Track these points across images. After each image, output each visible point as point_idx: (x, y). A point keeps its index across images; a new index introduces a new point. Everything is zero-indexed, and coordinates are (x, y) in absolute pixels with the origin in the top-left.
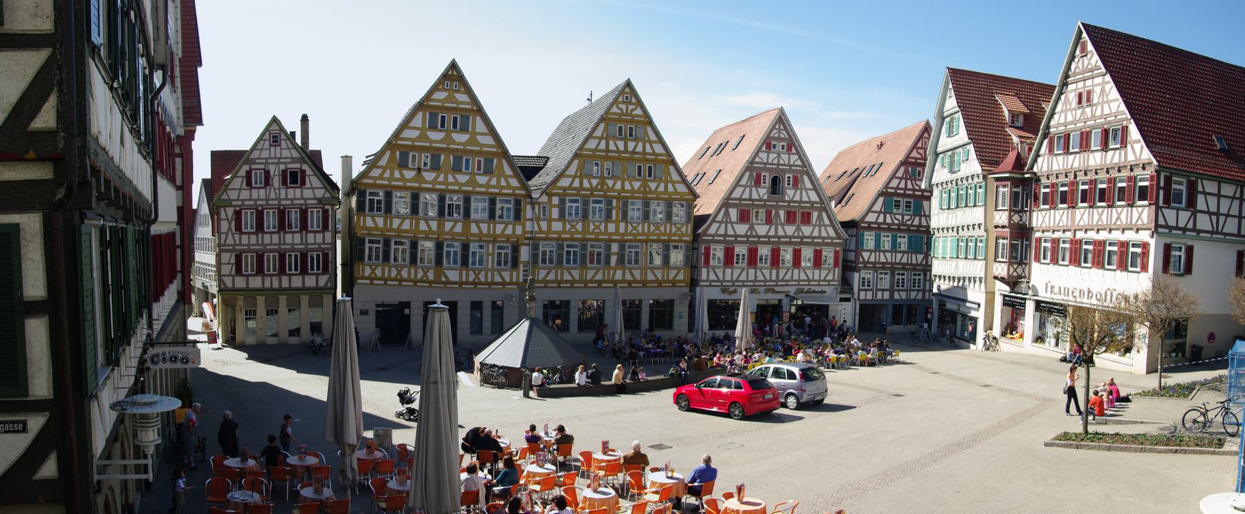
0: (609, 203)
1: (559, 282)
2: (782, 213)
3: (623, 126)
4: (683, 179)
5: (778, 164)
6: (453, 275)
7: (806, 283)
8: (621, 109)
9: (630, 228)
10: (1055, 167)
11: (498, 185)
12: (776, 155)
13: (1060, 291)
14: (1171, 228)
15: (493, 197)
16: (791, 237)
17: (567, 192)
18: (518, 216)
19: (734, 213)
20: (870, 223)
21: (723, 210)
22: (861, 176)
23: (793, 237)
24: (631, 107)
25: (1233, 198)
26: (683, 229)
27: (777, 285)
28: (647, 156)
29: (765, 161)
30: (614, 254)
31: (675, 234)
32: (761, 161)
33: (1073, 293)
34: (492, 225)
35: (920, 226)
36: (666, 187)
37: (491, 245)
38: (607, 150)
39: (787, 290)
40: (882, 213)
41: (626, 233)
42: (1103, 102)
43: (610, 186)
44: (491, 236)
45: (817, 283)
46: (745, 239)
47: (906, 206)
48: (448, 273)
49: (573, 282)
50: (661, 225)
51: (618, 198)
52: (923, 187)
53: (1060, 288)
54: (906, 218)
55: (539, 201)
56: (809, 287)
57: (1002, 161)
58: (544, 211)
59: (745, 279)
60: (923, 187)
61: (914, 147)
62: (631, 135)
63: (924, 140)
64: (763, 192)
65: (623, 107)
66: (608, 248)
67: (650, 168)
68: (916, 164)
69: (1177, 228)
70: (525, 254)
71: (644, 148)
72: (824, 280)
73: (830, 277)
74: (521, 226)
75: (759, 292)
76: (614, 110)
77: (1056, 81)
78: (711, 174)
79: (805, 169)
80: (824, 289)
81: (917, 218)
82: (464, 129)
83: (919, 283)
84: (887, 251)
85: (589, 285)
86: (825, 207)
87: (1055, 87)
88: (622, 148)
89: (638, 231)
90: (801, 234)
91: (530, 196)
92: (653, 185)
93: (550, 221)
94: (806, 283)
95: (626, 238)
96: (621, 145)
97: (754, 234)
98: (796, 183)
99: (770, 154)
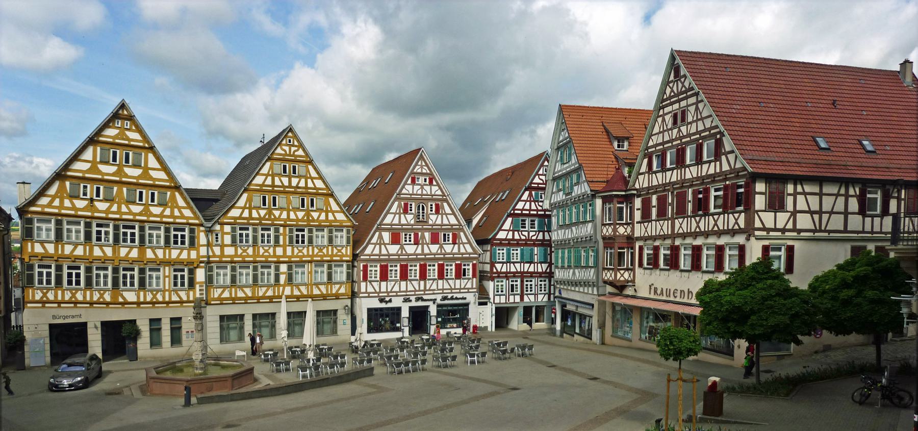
6: (131, 296)
7: (450, 291)
8: (285, 151)
10: (655, 183)
11: (172, 216)
14: (769, 230)
24: (293, 149)
26: (344, 251)
27: (425, 294)
30: (283, 273)
32: (407, 192)
35: (544, 239)
36: (327, 216)
38: (273, 185)
40: (511, 231)
41: (293, 256)
45: (458, 291)
48: (125, 294)
54: (531, 234)
56: (452, 295)
65: (287, 148)
66: (277, 269)
69: (776, 230)
70: (200, 275)
71: (306, 183)
72: (464, 288)
73: (469, 286)
74: (196, 252)
75: (411, 301)
82: (136, 165)
86: (462, 228)
89: (303, 253)
90: (443, 251)
93: (222, 246)
94: (450, 291)
95: (292, 259)
96: (285, 181)
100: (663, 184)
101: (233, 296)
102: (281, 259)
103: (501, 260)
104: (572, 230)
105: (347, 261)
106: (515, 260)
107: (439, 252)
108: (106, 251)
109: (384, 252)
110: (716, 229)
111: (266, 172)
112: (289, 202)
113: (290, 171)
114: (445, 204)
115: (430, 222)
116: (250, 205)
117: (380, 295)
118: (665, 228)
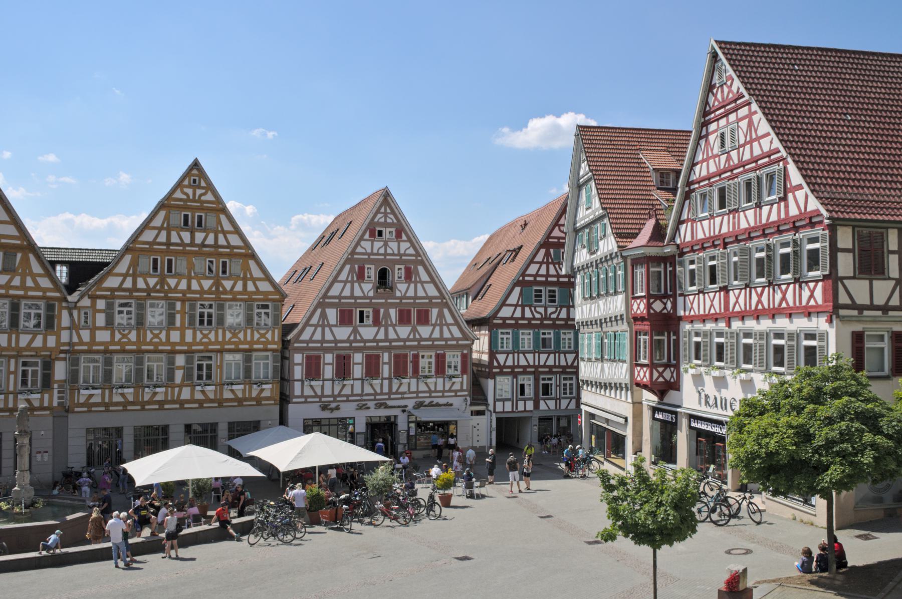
0: (172, 306)
1: (107, 405)
2: (393, 312)
3: (203, 215)
5: (386, 254)
7: (428, 395)
9: (199, 336)
10: (700, 236)
12: (382, 243)
13: (716, 403)
14: (861, 308)
15: (16, 301)
16: (404, 340)
17: (116, 293)
18: (50, 324)
19: (332, 315)
20: (504, 319)
21: (319, 311)
22: (501, 263)
23: (408, 340)
24: (199, 192)
27: (390, 399)
29: (369, 251)
31: (258, 342)
32: (364, 251)
33: (731, 406)
34: (14, 336)
36: (245, 286)
37: (13, 361)
38: (168, 243)
39: (403, 405)
41: (194, 343)
42: (751, 142)
43: (173, 286)
44: (13, 349)
45: (441, 394)
46: (348, 345)
47: (550, 296)
49: (126, 404)
51: (183, 301)
53: (716, 398)
54: (550, 310)
58: (86, 318)
59: (350, 393)
65: (190, 191)
66: (171, 361)
69: (872, 307)
70: (60, 371)
71: (216, 239)
72: (450, 391)
73: (457, 387)
75: (368, 408)
77: (688, 122)
79: (419, 258)
80: (450, 400)
83: (571, 389)
85: (147, 407)
86: (447, 302)
87: (691, 132)
89: (209, 339)
92: (228, 284)
93: (94, 329)
94: (428, 395)
95: (194, 348)
96: (186, 236)
97: (358, 338)
99: (375, 243)
100: (711, 237)
101: (107, 400)
102: (177, 348)
103: (505, 349)
104: (598, 306)
105: (273, 350)
106: (567, 349)
110: (784, 305)
112: (191, 266)
113: (193, 222)
114: (421, 269)
115: (398, 294)
117: (323, 399)
118: (716, 302)
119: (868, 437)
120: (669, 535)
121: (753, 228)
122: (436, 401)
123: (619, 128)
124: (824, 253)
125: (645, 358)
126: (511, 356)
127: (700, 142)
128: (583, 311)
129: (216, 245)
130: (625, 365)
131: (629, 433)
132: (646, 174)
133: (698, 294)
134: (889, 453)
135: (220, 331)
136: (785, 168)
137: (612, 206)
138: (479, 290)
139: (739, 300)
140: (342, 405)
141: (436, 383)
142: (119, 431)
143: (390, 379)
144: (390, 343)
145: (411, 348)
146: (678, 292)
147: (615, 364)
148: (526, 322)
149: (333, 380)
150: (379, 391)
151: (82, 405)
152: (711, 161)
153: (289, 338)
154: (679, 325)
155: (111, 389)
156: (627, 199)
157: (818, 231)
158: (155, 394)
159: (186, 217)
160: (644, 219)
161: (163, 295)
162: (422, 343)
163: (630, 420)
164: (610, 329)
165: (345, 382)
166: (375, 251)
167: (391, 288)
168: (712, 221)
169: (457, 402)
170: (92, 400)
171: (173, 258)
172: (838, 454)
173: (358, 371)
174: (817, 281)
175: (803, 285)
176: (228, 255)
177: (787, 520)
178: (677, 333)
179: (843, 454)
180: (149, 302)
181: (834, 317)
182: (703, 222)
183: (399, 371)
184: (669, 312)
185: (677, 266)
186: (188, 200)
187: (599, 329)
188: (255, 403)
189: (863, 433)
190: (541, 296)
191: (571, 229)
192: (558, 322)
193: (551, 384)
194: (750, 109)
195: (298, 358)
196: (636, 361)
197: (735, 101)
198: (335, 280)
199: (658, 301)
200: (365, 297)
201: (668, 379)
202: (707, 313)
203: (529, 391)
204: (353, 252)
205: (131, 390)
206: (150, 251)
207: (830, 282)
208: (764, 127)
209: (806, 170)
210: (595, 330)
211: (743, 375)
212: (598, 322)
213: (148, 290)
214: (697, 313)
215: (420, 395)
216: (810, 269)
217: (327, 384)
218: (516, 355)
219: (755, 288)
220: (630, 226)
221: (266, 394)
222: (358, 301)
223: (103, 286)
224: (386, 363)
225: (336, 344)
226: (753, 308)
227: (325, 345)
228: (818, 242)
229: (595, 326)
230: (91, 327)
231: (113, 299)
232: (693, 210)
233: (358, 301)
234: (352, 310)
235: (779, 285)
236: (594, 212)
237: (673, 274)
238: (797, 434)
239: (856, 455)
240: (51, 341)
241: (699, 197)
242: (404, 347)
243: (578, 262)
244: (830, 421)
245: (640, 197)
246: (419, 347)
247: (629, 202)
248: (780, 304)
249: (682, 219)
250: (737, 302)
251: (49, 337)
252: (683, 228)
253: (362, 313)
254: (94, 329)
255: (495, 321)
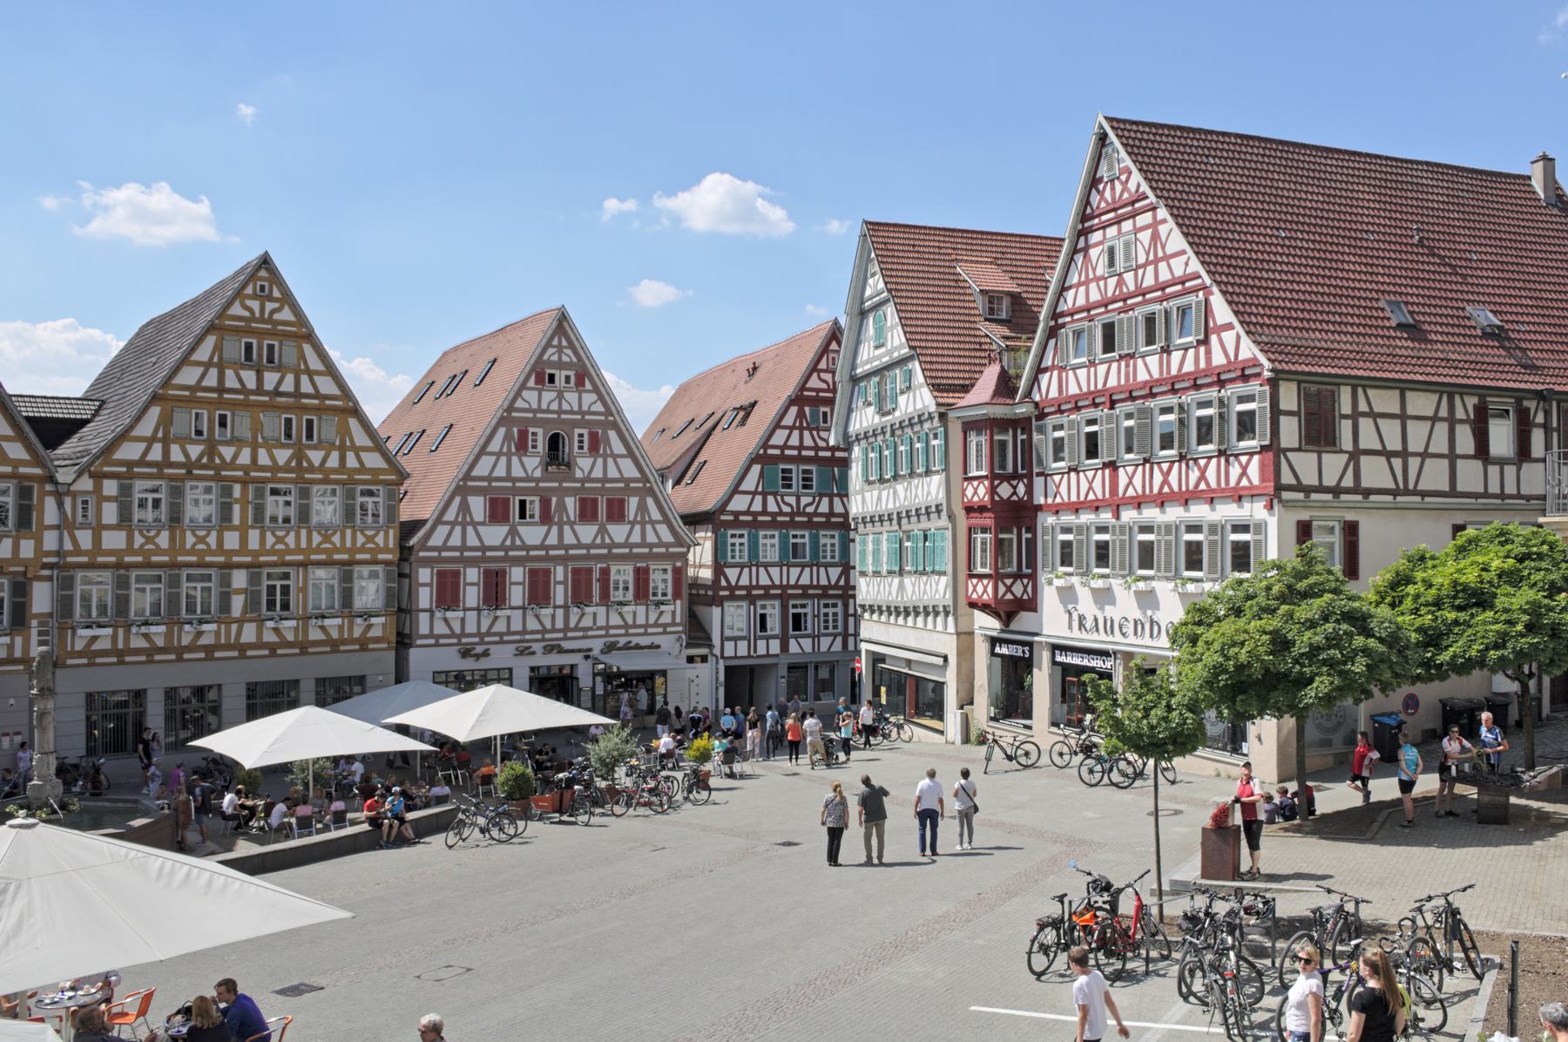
0: (227, 492)
1: (120, 654)
2: (570, 503)
4: (379, 445)
5: (560, 411)
7: (623, 631)
8: (250, 310)
10: (1073, 390)
12: (555, 394)
14: (1308, 490)
16: (588, 547)
18: (25, 519)
19: (478, 506)
20: (736, 514)
21: (457, 500)
22: (719, 428)
23: (593, 545)
24: (269, 306)
25: (1434, 419)
27: (566, 638)
28: (304, 401)
29: (535, 406)
31: (362, 550)
35: (831, 513)
36: (343, 459)
38: (221, 389)
39: (585, 647)
40: (760, 493)
41: (263, 550)
42: (1156, 261)
43: (228, 459)
45: (642, 631)
50: (335, 533)
51: (244, 482)
52: (832, 443)
53: (1096, 620)
55: (72, 488)
57: (973, 385)
59: (505, 630)
60: (832, 443)
61: (814, 369)
62: (271, 360)
63: (831, 355)
64: (533, 463)
65: (255, 305)
66: (226, 581)
67: (310, 423)
68: (817, 402)
69: (1321, 489)
70: (41, 598)
71: (297, 383)
72: (656, 625)
73: (666, 619)
75: (533, 653)
76: (236, 310)
77: (1062, 226)
78: (434, 433)
79: (611, 418)
80: (657, 640)
81: (825, 500)
83: (835, 621)
84: (773, 565)
85: (186, 656)
86: (651, 488)
87: (1063, 240)
88: (251, 383)
89: (286, 544)
91: (51, 479)
92: (315, 457)
93: (98, 529)
94: (623, 631)
95: (262, 559)
96: (249, 378)
98: (595, 445)
100: (1090, 393)
101: (120, 645)
102: (235, 559)
103: (737, 560)
104: (895, 492)
105: (387, 563)
106: (829, 559)
107: (598, 541)
108: (482, 534)
109: (472, 541)
110: (1203, 486)
111: (205, 358)
112: (257, 428)
113: (260, 355)
114: (612, 434)
115: (579, 474)
116: (166, 435)
117: (464, 640)
118: (1097, 485)
119: (1359, 641)
120: (1184, 744)
121: (1157, 380)
122: (635, 640)
123: (925, 228)
124: (1263, 416)
125: (983, 565)
126: (746, 570)
127: (1076, 257)
128: (863, 501)
129: (298, 394)
130: (944, 579)
131: (951, 679)
132: (967, 298)
133: (1068, 473)
134: (1383, 659)
135: (304, 533)
136: (1207, 301)
137: (923, 344)
138: (686, 468)
139: (1132, 480)
140: (493, 648)
141: (635, 613)
142: (139, 695)
143: (566, 607)
144: (567, 551)
145: (599, 558)
146: (1036, 470)
147: (925, 578)
148: (769, 518)
149: (478, 610)
150: (549, 626)
151: (80, 654)
152: (1093, 286)
153: (411, 543)
154: (1036, 517)
155: (128, 627)
156: (944, 334)
157: (1254, 387)
158: (199, 634)
159: (249, 347)
160: (980, 364)
161: (212, 472)
162: (615, 551)
163: (953, 660)
164: (916, 527)
165: (499, 613)
166: (544, 406)
167: (568, 465)
168: (1092, 369)
169: (667, 642)
170: (96, 646)
171: (229, 414)
172: (1324, 662)
173: (517, 595)
174: (1251, 454)
175: (1232, 459)
176: (317, 410)
177: (1209, 777)
178: (1032, 529)
179: (1330, 663)
180: (189, 484)
181: (1275, 501)
182: (1078, 371)
183: (580, 596)
184: (1021, 500)
185: (1034, 434)
186: (253, 319)
187: (897, 528)
188: (357, 647)
189: (1352, 637)
190: (791, 479)
191: (846, 377)
192: (815, 519)
193: (805, 614)
194: (1155, 217)
195: (424, 575)
196: (970, 570)
197: (1133, 203)
198: (482, 451)
199: (1005, 484)
200: (528, 479)
201: (1019, 596)
202: (1082, 499)
203: (774, 625)
204: (511, 408)
205: (162, 629)
206: (192, 401)
207: (1270, 455)
208: (1176, 240)
209: (1237, 304)
210: (888, 528)
211: (1141, 585)
212: (895, 516)
213: (189, 466)
214: (1066, 500)
215: (612, 632)
216: (1240, 437)
217: (470, 618)
218: (754, 569)
219: (1159, 463)
220: (950, 375)
221: (376, 632)
222: (518, 484)
223: (114, 457)
224: (560, 583)
225: (484, 553)
226: (1156, 491)
227: (466, 554)
228: (1254, 401)
229: (886, 523)
230: (94, 524)
231: (131, 478)
232: (1062, 354)
233: (518, 484)
234: (508, 499)
235: (1195, 460)
236: (890, 352)
237: (1028, 446)
238: (1273, 641)
239: (1345, 663)
240: (27, 549)
241: (1071, 334)
242: (588, 557)
243: (858, 426)
244: (1311, 624)
245: (962, 332)
246: (610, 557)
247: (946, 338)
248: (1197, 485)
249: (1043, 366)
250: (1130, 483)
251: (23, 542)
252: (1044, 378)
253: (523, 504)
254: (98, 529)
255: (723, 517)
